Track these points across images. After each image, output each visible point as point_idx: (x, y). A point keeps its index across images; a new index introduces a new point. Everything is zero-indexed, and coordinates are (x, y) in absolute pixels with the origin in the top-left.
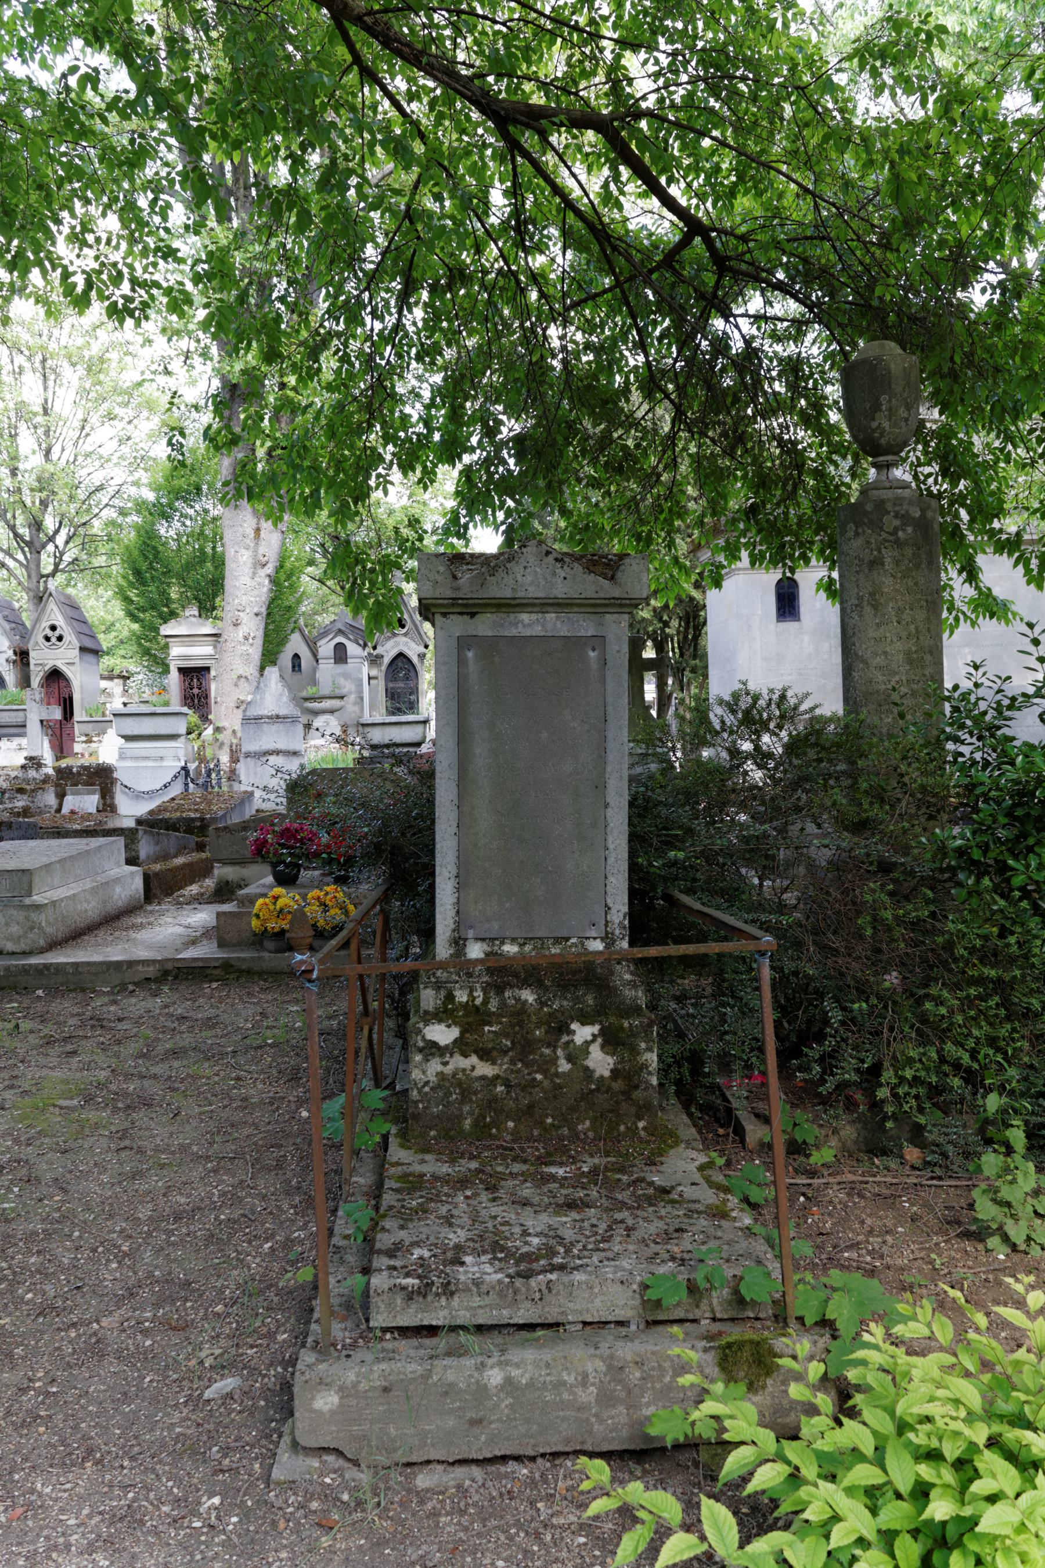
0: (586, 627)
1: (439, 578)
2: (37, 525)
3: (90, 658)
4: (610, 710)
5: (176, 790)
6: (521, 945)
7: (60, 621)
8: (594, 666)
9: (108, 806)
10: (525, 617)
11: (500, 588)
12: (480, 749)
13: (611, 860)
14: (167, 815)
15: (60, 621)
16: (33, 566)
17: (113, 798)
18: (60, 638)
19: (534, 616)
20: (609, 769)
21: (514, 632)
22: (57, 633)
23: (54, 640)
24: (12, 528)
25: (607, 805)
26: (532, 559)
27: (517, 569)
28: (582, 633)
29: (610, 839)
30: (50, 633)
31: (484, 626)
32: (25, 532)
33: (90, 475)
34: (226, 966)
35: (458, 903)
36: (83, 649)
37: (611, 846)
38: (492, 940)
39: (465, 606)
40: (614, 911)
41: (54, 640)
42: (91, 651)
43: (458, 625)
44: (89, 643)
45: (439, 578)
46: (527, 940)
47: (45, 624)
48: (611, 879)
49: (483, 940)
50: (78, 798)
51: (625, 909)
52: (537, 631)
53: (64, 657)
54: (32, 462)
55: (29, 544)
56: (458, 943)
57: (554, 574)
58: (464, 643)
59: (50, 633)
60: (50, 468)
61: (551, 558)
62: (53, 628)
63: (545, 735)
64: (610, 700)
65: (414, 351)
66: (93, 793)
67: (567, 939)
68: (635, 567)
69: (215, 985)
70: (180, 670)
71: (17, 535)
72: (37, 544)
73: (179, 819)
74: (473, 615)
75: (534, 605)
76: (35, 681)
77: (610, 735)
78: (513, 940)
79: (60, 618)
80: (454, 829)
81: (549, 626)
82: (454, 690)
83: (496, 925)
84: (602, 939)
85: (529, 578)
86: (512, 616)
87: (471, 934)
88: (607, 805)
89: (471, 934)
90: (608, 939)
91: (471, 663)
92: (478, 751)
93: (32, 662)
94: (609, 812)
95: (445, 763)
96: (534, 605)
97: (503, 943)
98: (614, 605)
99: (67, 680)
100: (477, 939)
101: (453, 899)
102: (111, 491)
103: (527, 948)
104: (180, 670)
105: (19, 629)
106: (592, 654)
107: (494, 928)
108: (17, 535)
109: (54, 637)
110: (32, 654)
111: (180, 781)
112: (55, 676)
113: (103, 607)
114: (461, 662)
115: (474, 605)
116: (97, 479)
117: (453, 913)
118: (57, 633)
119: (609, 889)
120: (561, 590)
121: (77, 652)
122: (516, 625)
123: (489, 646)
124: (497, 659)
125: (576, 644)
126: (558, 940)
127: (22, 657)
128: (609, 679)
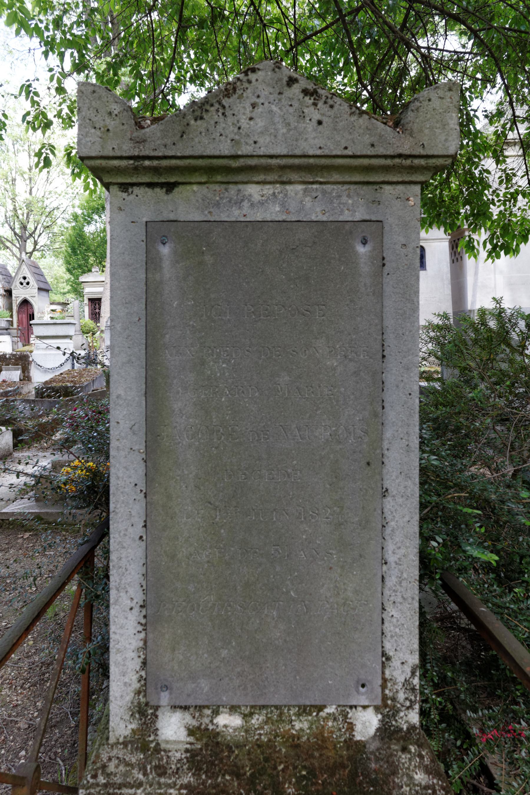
0: (352, 206)
1: (111, 123)
2: (24, 228)
3: (44, 293)
4: (390, 340)
5: (68, 367)
6: (246, 717)
7: (29, 275)
8: (365, 268)
9: (26, 378)
10: (253, 191)
11: (213, 141)
12: (182, 405)
13: (391, 581)
14: (54, 384)
15: (29, 275)
16: (22, 249)
17: (29, 372)
18: (28, 283)
19: (268, 190)
20: (388, 434)
21: (236, 214)
22: (26, 281)
23: (25, 284)
24: (13, 230)
25: (385, 493)
26: (265, 91)
27: (240, 107)
28: (346, 216)
29: (390, 547)
30: (23, 281)
31: (188, 204)
32: (18, 231)
33: (51, 203)
34: (38, 517)
35: (144, 663)
36: (40, 289)
37: (391, 559)
38: (200, 708)
39: (156, 170)
40: (396, 663)
41: (25, 284)
42: (44, 289)
43: (148, 204)
44: (43, 286)
45: (111, 123)
46: (255, 709)
47: (21, 276)
48: (391, 610)
49: (185, 708)
50: (9, 372)
51: (415, 659)
52: (274, 212)
53: (30, 293)
54: (22, 196)
55: (21, 237)
56: (145, 713)
57: (302, 116)
58: (156, 232)
59: (23, 281)
60: (31, 199)
61: (296, 89)
62: (25, 278)
63: (284, 379)
64: (389, 322)
65: (188, 75)
66: (18, 370)
67: (321, 708)
68: (436, 103)
69: (27, 535)
70: (89, 299)
71: (15, 234)
72: (24, 237)
73: (61, 387)
74: (170, 187)
75: (267, 169)
76: (15, 308)
77: (390, 379)
78: (233, 709)
79: (28, 273)
80: (139, 530)
81: (293, 206)
82: (139, 307)
83: (205, 685)
84: (377, 709)
85: (260, 123)
86: (233, 189)
87: (165, 699)
88: (385, 493)
89: (165, 699)
90: (387, 708)
91: (166, 264)
92: (177, 406)
93: (13, 295)
94: (389, 504)
95: (125, 425)
96: (267, 169)
97: (216, 713)
98: (400, 169)
99: (31, 305)
100: (174, 707)
101: (136, 642)
102: (62, 210)
103: (256, 720)
104: (89, 299)
105: (9, 279)
106: (361, 249)
107: (203, 690)
108: (15, 234)
109: (25, 282)
110: (13, 292)
111: (69, 363)
112: (25, 303)
113: (54, 267)
114: (152, 262)
115: (171, 170)
116: (54, 205)
117: (136, 664)
118: (26, 281)
119: (388, 627)
120: (313, 142)
121: (37, 290)
122: (239, 203)
123: (194, 238)
124: (208, 259)
125: (337, 232)
126: (304, 710)
127: (9, 293)
128: (388, 289)
